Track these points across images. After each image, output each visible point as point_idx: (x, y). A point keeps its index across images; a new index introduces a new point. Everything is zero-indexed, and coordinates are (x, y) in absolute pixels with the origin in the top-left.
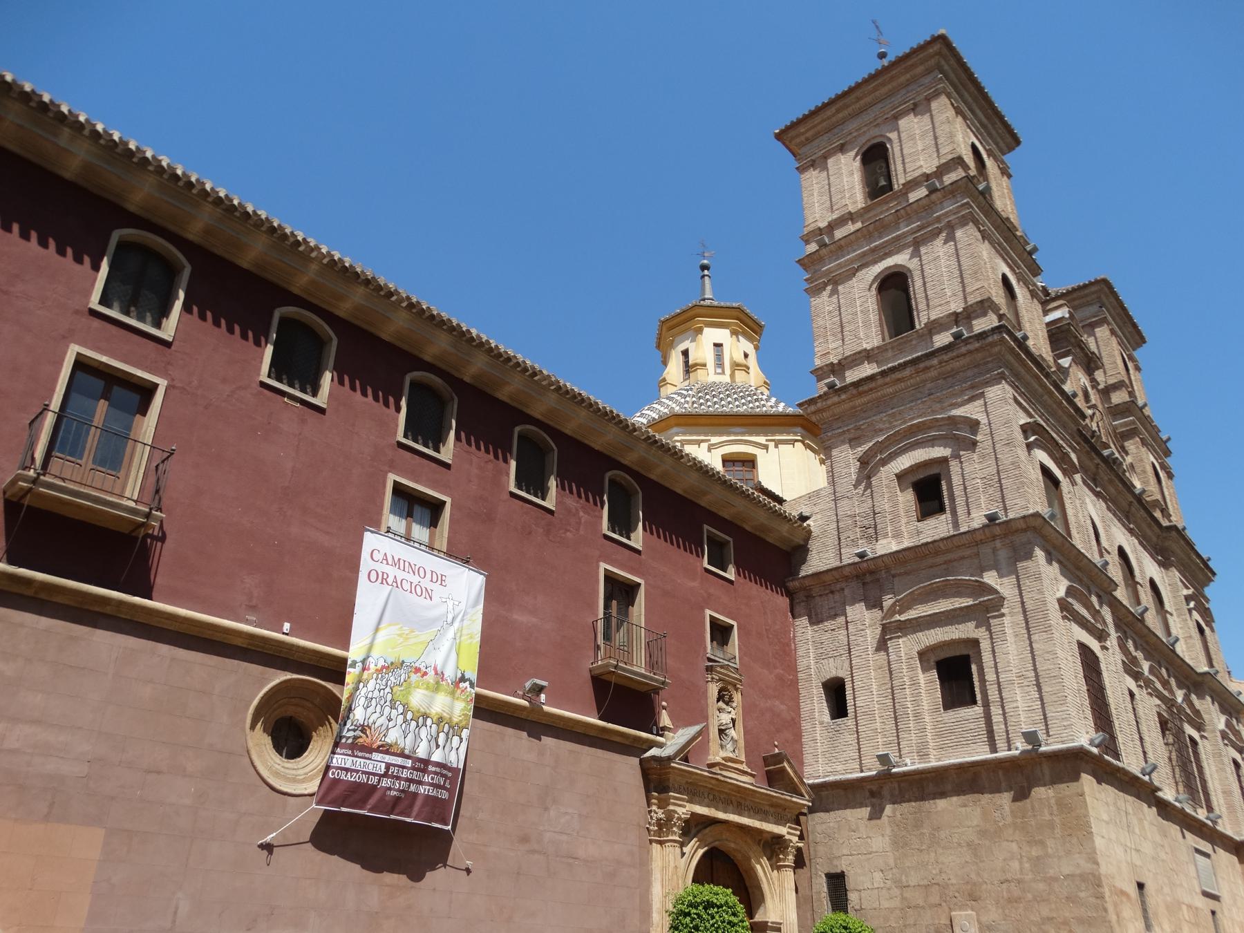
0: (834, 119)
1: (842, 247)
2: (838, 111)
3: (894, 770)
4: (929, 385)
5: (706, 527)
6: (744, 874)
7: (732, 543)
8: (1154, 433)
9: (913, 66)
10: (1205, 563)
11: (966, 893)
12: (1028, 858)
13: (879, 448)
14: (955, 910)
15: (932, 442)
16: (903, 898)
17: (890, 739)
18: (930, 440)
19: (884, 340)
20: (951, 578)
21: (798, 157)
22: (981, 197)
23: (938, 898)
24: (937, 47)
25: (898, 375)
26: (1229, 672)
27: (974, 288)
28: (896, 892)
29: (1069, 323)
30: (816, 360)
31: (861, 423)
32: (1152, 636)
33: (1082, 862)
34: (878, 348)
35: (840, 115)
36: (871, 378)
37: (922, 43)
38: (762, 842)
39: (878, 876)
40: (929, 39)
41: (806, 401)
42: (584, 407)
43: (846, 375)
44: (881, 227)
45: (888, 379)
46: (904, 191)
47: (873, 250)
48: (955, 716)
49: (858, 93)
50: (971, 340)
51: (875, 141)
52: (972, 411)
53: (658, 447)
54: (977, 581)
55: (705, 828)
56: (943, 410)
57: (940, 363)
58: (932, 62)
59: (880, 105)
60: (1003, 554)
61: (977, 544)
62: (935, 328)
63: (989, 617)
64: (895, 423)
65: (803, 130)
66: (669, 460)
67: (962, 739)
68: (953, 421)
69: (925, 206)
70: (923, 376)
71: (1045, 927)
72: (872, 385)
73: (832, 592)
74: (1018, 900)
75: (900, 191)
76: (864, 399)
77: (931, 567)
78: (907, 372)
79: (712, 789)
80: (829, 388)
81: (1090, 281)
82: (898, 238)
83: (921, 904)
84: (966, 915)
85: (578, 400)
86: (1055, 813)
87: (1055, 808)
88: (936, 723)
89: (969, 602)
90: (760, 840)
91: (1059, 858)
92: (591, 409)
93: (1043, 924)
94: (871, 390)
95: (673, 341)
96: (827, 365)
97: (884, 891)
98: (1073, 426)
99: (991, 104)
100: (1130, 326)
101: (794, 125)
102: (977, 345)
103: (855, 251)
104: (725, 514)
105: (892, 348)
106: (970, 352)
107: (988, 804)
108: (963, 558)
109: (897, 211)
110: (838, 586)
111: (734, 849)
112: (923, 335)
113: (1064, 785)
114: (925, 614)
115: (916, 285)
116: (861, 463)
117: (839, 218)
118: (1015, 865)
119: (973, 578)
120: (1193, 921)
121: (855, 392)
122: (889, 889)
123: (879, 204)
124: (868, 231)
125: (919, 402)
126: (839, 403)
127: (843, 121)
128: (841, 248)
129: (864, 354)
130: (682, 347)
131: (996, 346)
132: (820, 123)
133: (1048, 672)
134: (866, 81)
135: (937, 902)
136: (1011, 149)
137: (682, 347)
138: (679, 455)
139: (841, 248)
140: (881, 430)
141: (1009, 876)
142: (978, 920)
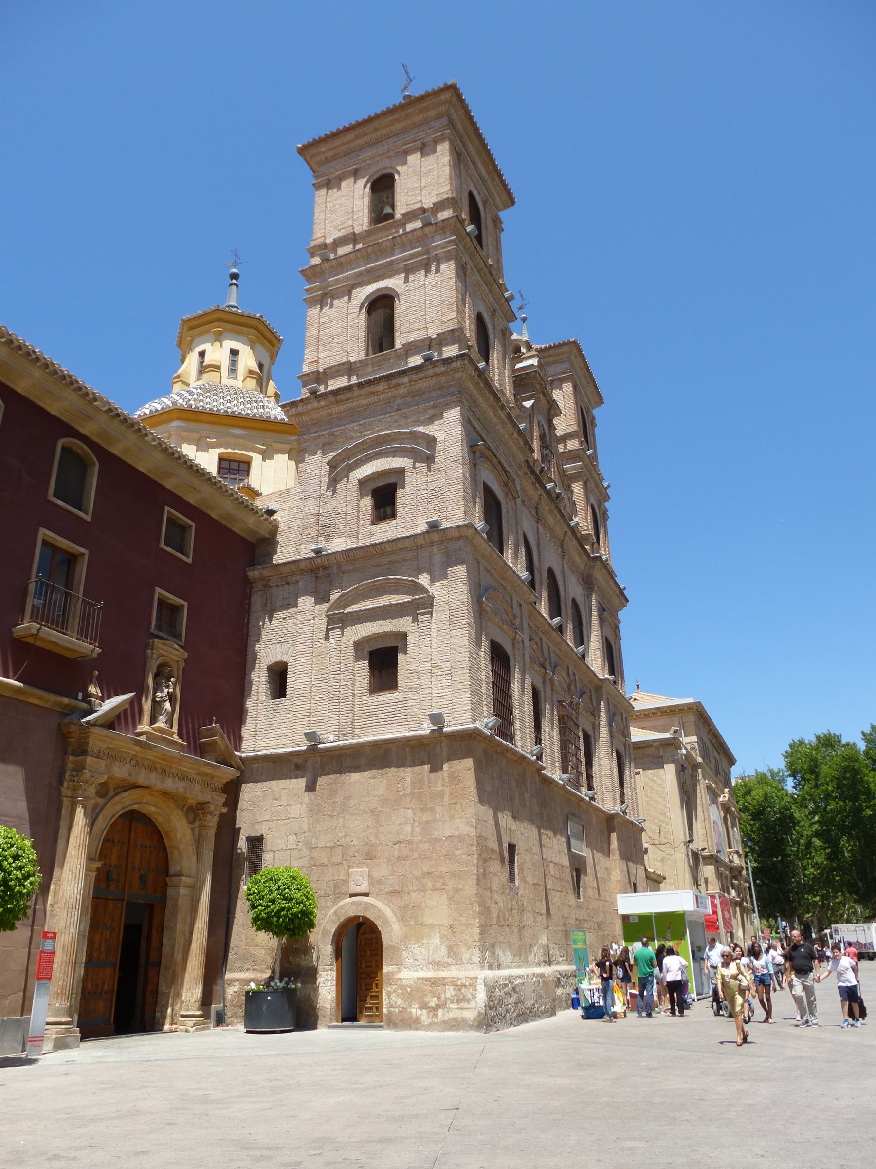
0: (352, 145)
1: (342, 264)
2: (357, 137)
3: (320, 746)
4: (399, 401)
5: (167, 508)
6: (163, 835)
7: (194, 528)
8: (597, 479)
9: (427, 109)
10: (621, 592)
11: (364, 853)
12: (419, 822)
13: (348, 454)
14: (353, 867)
15: (394, 453)
16: (311, 858)
17: (319, 718)
18: (392, 452)
19: (367, 354)
20: (391, 577)
21: (317, 174)
22: (467, 238)
23: (340, 857)
24: (447, 96)
25: (373, 389)
26: (638, 686)
27: (449, 318)
28: (306, 852)
29: (536, 371)
30: (304, 366)
31: (335, 430)
32: (564, 644)
33: (462, 826)
34: (360, 362)
35: (359, 142)
36: (349, 388)
37: (436, 89)
38: (185, 809)
39: (292, 839)
40: (442, 86)
41: (288, 404)
42: (39, 367)
43: (329, 384)
44: (380, 251)
45: (363, 391)
46: (403, 221)
47: (369, 271)
48: (378, 700)
49: (376, 124)
50: (438, 364)
51: (386, 172)
52: (430, 430)
53: (120, 421)
54: (412, 581)
55: (124, 791)
56: (407, 425)
57: (410, 382)
58: (443, 109)
59: (393, 139)
60: (438, 558)
61: (419, 547)
62: (411, 350)
63: (418, 614)
64: (365, 433)
65: (323, 149)
66: (132, 437)
67: (381, 720)
68: (415, 437)
69: (419, 238)
70: (395, 392)
71: (424, 881)
72: (349, 395)
73: (288, 583)
74: (406, 858)
75: (400, 220)
76: (342, 408)
77: (377, 566)
78: (381, 387)
79: (135, 755)
80: (311, 393)
81: (563, 342)
82: (391, 263)
83: (326, 863)
84: (361, 871)
85: (33, 358)
86: (446, 784)
87: (447, 780)
88: (361, 706)
89: (406, 598)
90: (184, 806)
91: (444, 822)
92: (47, 371)
93: (423, 878)
94: (348, 399)
95: (192, 341)
96: (312, 372)
97: (296, 852)
98: (521, 457)
99: (493, 161)
100: (592, 386)
101: (316, 143)
102: (443, 369)
103: (353, 269)
104: (191, 499)
105: (373, 364)
106: (436, 375)
107: (393, 776)
108: (404, 560)
109: (393, 238)
110: (294, 579)
111: (155, 813)
112: (400, 356)
113: (457, 762)
114: (365, 608)
115: (400, 307)
116: (330, 467)
117: (344, 236)
118: (408, 828)
119: (409, 578)
120: (558, 876)
121: (333, 399)
122: (300, 850)
123: (380, 229)
124: (367, 252)
125: (388, 415)
126: (318, 409)
127: (360, 149)
128: (341, 264)
129: (347, 366)
130: (200, 348)
131: (458, 372)
132: (339, 146)
133: (458, 664)
134: (384, 114)
135: (340, 861)
136: (506, 207)
137: (200, 348)
138: (144, 432)
139: (341, 264)
140: (352, 439)
141: (401, 838)
142: (370, 876)
